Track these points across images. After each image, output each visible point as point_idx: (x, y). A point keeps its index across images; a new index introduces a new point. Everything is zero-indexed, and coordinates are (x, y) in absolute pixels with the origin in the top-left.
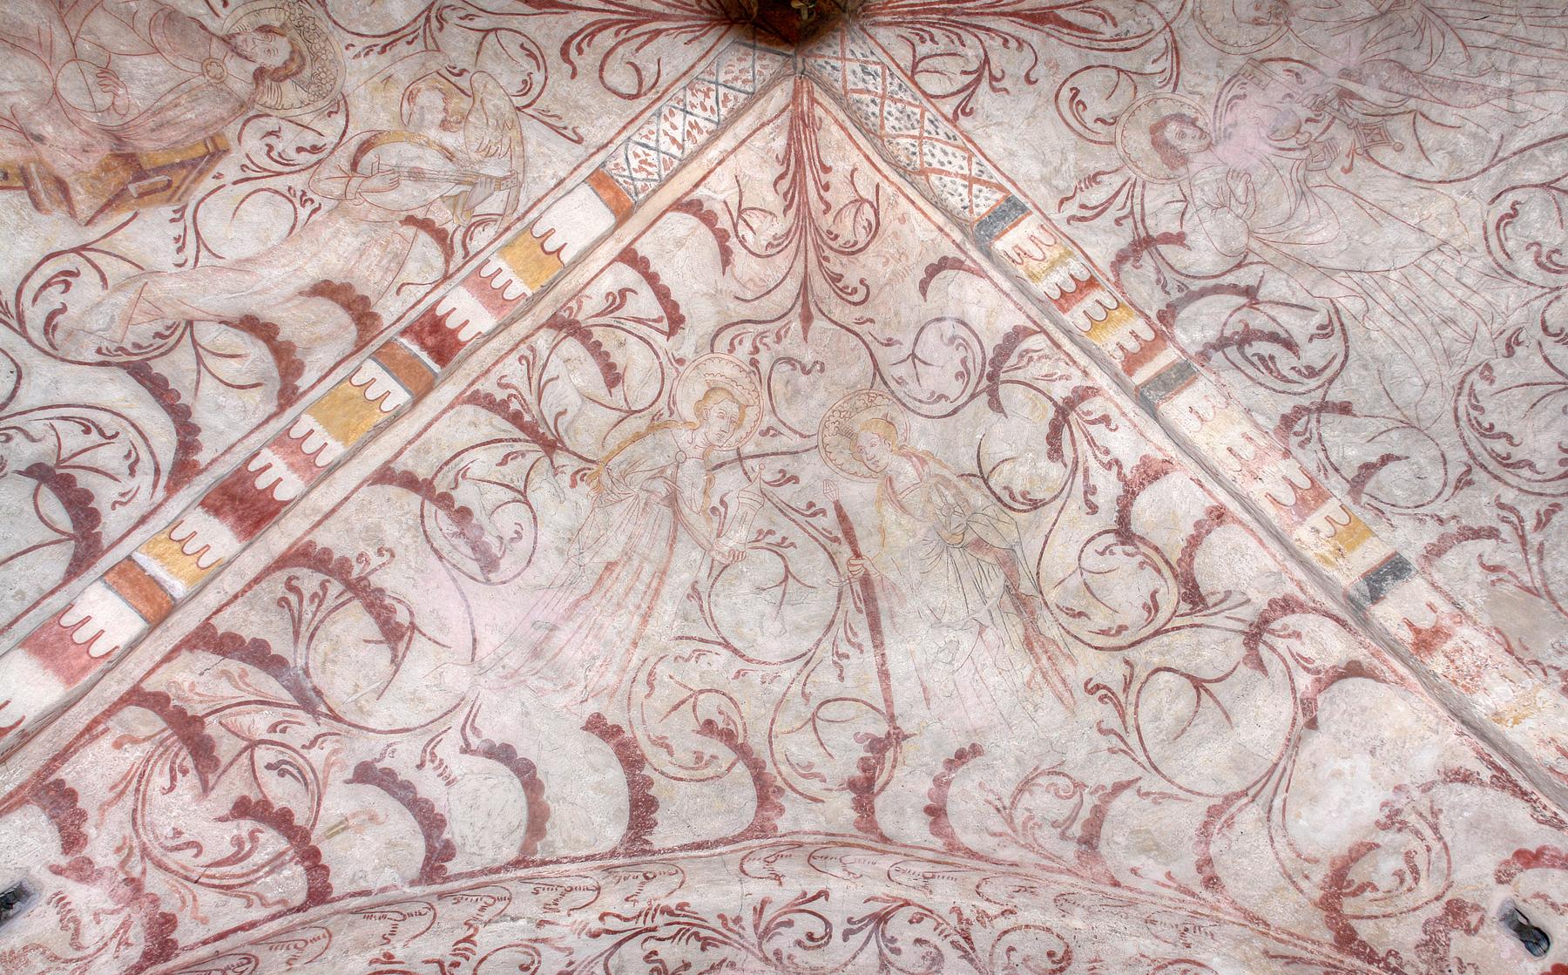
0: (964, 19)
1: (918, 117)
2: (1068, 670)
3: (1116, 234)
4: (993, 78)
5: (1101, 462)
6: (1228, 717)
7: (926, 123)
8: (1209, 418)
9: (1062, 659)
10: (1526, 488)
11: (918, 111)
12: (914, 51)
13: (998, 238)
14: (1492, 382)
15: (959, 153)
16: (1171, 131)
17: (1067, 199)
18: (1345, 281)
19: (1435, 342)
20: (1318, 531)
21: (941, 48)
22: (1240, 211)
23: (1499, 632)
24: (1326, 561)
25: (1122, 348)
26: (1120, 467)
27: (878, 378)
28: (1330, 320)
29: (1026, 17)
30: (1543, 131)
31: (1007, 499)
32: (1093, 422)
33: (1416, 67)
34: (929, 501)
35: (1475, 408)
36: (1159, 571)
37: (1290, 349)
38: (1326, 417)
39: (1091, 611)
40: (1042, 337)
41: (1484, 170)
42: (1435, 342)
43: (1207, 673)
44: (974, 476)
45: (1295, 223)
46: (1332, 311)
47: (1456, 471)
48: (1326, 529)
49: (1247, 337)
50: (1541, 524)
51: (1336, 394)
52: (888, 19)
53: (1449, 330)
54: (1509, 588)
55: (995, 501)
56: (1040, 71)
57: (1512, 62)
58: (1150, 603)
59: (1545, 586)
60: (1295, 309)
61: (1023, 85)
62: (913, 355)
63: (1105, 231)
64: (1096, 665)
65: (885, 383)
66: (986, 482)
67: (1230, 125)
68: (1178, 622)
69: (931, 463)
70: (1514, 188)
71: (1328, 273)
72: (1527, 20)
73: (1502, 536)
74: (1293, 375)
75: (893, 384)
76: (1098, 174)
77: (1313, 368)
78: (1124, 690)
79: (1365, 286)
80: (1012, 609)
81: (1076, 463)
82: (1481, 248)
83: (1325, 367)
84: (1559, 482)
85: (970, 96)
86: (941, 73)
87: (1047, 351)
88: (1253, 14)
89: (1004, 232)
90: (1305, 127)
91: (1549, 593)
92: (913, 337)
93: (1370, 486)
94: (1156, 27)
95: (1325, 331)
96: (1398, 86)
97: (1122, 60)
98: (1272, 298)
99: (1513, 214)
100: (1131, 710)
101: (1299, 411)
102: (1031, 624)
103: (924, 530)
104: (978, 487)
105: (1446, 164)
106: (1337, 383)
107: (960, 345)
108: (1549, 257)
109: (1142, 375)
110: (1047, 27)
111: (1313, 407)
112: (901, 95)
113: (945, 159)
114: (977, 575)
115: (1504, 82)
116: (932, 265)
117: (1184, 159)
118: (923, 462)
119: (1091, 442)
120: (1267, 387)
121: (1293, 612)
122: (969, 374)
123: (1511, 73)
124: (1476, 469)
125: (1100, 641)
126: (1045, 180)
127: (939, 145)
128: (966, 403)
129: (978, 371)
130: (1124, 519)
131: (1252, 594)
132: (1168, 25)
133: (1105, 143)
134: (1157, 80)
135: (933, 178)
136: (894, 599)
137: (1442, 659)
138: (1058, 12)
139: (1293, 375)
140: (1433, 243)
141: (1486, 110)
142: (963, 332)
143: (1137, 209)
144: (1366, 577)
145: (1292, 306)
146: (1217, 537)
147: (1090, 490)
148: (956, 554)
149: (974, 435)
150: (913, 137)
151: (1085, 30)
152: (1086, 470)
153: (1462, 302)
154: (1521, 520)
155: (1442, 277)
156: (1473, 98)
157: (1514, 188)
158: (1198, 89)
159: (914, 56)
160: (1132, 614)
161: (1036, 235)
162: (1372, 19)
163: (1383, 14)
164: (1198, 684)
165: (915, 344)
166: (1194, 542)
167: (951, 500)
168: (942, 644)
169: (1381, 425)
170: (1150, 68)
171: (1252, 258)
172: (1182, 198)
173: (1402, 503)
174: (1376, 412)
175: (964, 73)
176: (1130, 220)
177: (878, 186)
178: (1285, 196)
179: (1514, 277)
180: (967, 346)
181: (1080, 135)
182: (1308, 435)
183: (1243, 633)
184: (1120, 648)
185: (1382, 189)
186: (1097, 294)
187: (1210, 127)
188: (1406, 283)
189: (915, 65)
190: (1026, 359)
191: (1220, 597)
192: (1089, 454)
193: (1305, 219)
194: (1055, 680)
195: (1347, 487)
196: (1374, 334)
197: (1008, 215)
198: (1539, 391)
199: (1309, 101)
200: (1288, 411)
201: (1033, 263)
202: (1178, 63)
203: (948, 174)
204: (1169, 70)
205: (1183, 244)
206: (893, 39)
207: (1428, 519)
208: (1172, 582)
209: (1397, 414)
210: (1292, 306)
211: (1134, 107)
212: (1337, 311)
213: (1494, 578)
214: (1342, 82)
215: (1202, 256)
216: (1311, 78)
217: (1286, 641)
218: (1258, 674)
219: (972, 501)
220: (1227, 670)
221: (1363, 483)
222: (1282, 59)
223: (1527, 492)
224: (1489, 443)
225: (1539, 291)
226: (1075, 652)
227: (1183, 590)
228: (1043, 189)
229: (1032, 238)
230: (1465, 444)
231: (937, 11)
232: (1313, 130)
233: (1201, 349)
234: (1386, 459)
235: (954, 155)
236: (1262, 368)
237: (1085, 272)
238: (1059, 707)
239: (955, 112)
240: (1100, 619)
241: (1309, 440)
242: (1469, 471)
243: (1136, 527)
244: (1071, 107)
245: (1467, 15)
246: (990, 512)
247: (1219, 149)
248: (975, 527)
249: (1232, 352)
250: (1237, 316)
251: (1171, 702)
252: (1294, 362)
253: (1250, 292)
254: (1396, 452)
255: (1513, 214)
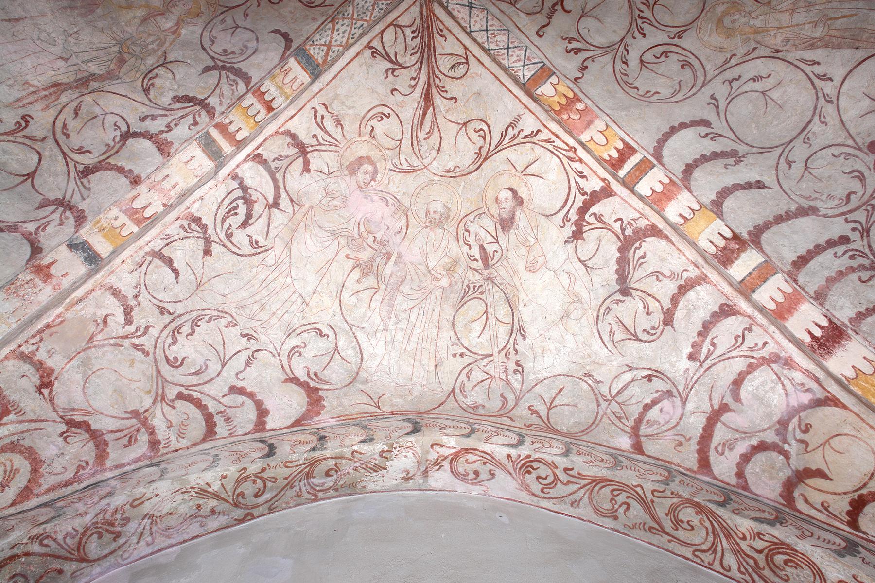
0: (426, 56)
1: (364, 18)
2: (39, 106)
3: (307, 134)
4: (394, 70)
5: (171, 122)
6: (6, 190)
7: (362, 23)
8: (188, 166)
9: (46, 103)
10: (159, 340)
11: (368, 18)
12: (407, 27)
13: (296, 59)
14: (226, 327)
15: (344, 40)
16: (370, 168)
17: (327, 108)
18: (283, 256)
19: (251, 300)
20: (116, 219)
21: (409, 41)
22: (324, 202)
23: (62, 322)
24: (96, 223)
25: (231, 123)
26: (167, 132)
27: (225, 9)
28: (261, 247)
29: (428, 90)
30: (365, 345)
31: (150, 75)
32: (194, 117)
33: (401, 288)
34: (150, 35)
35: (210, 319)
36: (103, 154)
37: (242, 224)
38: (201, 242)
39: (79, 120)
40: (245, 90)
41: (346, 321)
42: (251, 300)
43: (37, 181)
44: (165, 59)
45: (317, 230)
46: (266, 248)
47: (170, 307)
48: (117, 224)
49: (249, 202)
50: (135, 346)
51: (216, 248)
52: (425, 13)
53: (258, 307)
54: (92, 328)
55: (149, 70)
56: (398, 97)
57: (402, 329)
58: (84, 150)
59: (95, 347)
60: (267, 228)
61: (391, 87)
62: (238, 27)
63: (309, 128)
64: (42, 121)
65: (222, 13)
66: (161, 65)
67: (372, 199)
68: (71, 164)
69: (173, 37)
70: (336, 334)
71: (288, 245)
72: (421, 334)
73: (127, 327)
74: (226, 226)
75: (221, 17)
76: (342, 126)
77: (231, 236)
78: (25, 136)
79: (282, 265)
80: (79, 77)
81: (171, 110)
82: (304, 322)
83: (233, 243)
84: (163, 356)
85: (383, 57)
86: (395, 41)
87: (236, 93)
88: (432, 211)
89: (299, 63)
90: (371, 236)
91: (90, 348)
92: (248, 27)
93: (157, 261)
94: (425, 161)
95: (254, 244)
96: (392, 280)
97: (406, 142)
98: (272, 216)
99: (321, 335)
100: (11, 138)
101: (204, 227)
102: (69, 87)
103: (131, 31)
104: (158, 61)
105: (351, 303)
106: (224, 249)
107: (243, 51)
108: (297, 352)
109: (215, 134)
110: (423, 102)
111: (207, 235)
112: (377, 9)
113: (341, 31)
114: (102, 59)
115: (391, 327)
116: (289, 35)
117: (352, 173)
118: (174, 32)
119: (182, 117)
120: (218, 210)
121: (76, 221)
122: (226, 55)
123: (396, 329)
124: (171, 317)
125: (59, 125)
126: (336, 96)
127: (348, 29)
128: (209, 55)
129: (227, 60)
130: (136, 135)
131: (87, 201)
132: (426, 167)
133: (360, 131)
134: (396, 161)
135: (330, 25)
136: (83, 11)
137: (29, 277)
138: (431, 108)
139: (226, 226)
140: (307, 299)
141: (378, 320)
142: (250, 52)
143: (323, 148)
144: (86, 242)
145: (269, 227)
146: (124, 181)
147: (154, 118)
148: (116, 48)
149: (189, 59)
150: (353, 15)
151: (422, 123)
152: (166, 115)
153: (274, 313)
154: (137, 337)
155: (288, 304)
156: (384, 314)
157: (336, 334)
158: (392, 183)
159: (404, 26)
160: (76, 141)
161: (298, 80)
162: (427, 267)
163: (429, 271)
164: (31, 175)
165: (244, 28)
166: (120, 170)
167: (150, 47)
168: (53, 35)
169: (198, 270)
170: (402, 157)
171: (297, 208)
172: (330, 172)
173: (147, 278)
174: (206, 269)
175: (396, 54)
176: (316, 143)
177: (333, 5)
178: (332, 225)
179: (287, 337)
180: (241, 54)
181: (364, 118)
182: (189, 231)
183: (64, 198)
184: (54, 134)
185: (337, 273)
186: (263, 111)
187: (371, 188)
188: (284, 287)
189: (400, 27)
190: (233, 83)
191: (87, 185)
192: (176, 116)
193: (319, 235)
194: (31, 98)
195: (157, 249)
196: (254, 270)
197: (309, 65)
198: (220, 348)
199: (386, 238)
200: (204, 221)
201: (281, 77)
202: (405, 172)
203: (332, 33)
204: (402, 167)
205: (303, 171)
206: (413, 15)
207: (138, 290)
208: (97, 160)
209: (205, 279)
210: (269, 227)
211: (381, 148)
212: (266, 250)
213: (99, 321)
214: (395, 253)
215: (295, 180)
216: (398, 239)
217: (58, 218)
218: (37, 205)
219: (149, 58)
220: (40, 190)
221: (160, 258)
222: (408, 225)
223: (157, 341)
224: (189, 323)
225: (278, 348)
226: (51, 111)
227: (91, 166)
228: (332, 95)
229: (296, 78)
230: (187, 313)
231: (429, 41)
232: (370, 240)
233: (240, 176)
234: (176, 272)
235: (343, 37)
236: (229, 208)
237: (277, 106)
238: (11, 99)
239: (374, 48)
240: (73, 124)
241: (186, 231)
242: (169, 313)
243: (130, 142)
244: (379, 113)
245: (426, 308)
246: (142, 67)
247: (358, 192)
248: (133, 59)
249: (239, 193)
250: (261, 197)
251: (17, 160)
252: (234, 226)
253: (276, 204)
254: (181, 278)
255: (321, 335)
